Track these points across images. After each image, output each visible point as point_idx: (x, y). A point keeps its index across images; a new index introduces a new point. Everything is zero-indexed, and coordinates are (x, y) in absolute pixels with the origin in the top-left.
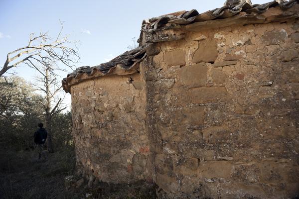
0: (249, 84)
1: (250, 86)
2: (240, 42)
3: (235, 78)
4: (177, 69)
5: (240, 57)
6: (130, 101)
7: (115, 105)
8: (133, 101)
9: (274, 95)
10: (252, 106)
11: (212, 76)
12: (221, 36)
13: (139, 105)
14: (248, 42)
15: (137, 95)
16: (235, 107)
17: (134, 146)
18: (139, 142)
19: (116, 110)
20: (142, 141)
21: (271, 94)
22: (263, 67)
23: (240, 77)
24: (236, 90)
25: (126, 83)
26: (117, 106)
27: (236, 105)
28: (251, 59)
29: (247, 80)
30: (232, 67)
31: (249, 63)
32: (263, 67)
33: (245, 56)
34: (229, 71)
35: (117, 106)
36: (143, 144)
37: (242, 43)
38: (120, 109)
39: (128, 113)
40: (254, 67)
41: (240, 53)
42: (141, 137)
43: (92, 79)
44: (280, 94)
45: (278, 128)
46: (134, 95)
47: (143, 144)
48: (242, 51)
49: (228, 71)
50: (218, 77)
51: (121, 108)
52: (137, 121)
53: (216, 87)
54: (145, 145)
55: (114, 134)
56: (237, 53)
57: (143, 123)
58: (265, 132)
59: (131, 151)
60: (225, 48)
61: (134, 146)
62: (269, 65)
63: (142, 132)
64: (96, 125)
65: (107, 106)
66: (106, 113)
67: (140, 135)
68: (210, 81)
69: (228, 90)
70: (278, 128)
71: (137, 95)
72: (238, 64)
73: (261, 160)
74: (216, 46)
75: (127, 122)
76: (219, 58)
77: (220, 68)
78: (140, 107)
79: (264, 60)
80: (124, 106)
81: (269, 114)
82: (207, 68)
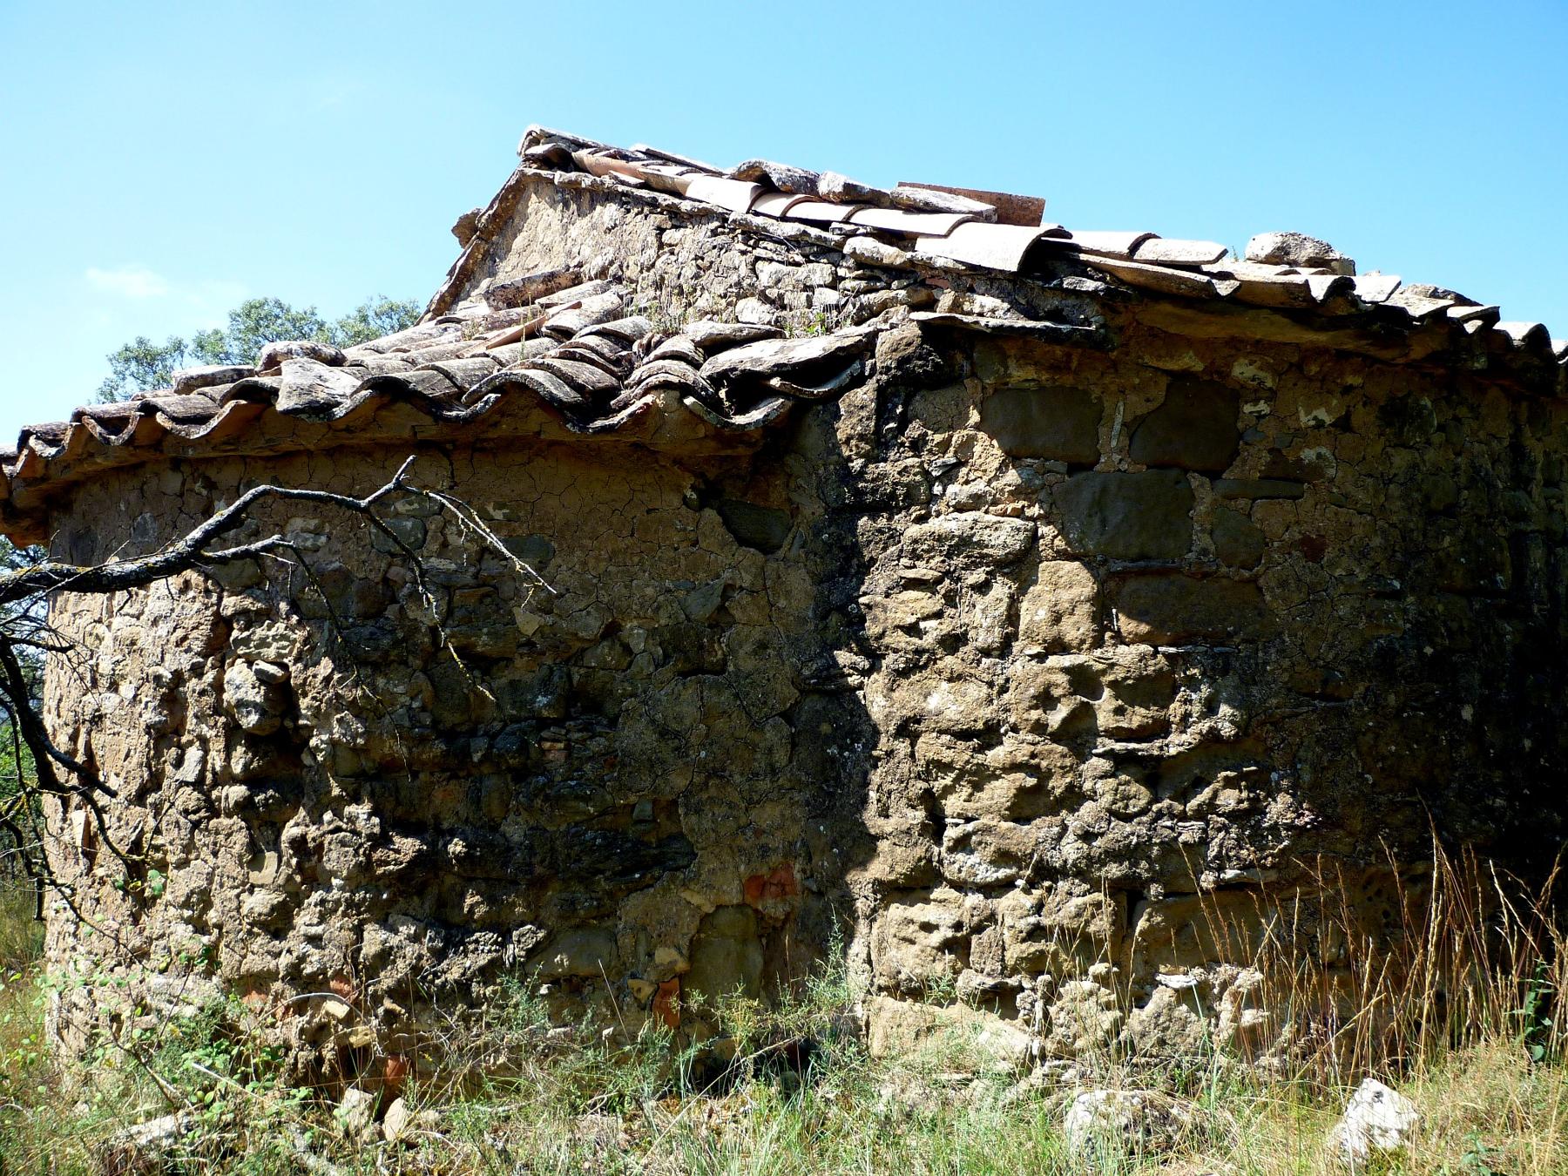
0: (1339, 580)
1: (1342, 589)
2: (1322, 414)
3: (1295, 553)
4: (1051, 478)
5: (1315, 470)
6: (701, 608)
7: (593, 624)
8: (722, 609)
9: (1405, 632)
10: (1343, 668)
11: (1211, 533)
12: (1262, 374)
13: (757, 634)
14: (1344, 424)
15: (747, 580)
16: (1293, 665)
17: (714, 864)
18: (741, 841)
19: (606, 653)
20: (759, 833)
21: (1397, 628)
22: (1380, 523)
23: (1312, 549)
24: (1296, 598)
25: (676, 501)
26: (612, 631)
27: (1298, 658)
28: (1350, 488)
29: (1333, 564)
30: (1288, 505)
31: (1343, 501)
32: (1380, 523)
33: (1331, 472)
34: (1273, 518)
35: (612, 631)
36: (765, 851)
37: (1328, 420)
38: (627, 649)
39: (684, 674)
40: (1356, 519)
41: (1319, 456)
42: (754, 814)
43: (85, 585)
44: (1423, 629)
45: (1411, 750)
46: (727, 575)
47: (765, 851)
48: (1323, 450)
49: (1273, 520)
50: (1236, 540)
51: (638, 645)
52: (738, 720)
53: (1225, 582)
54: (775, 859)
55: (587, 799)
56: (1309, 455)
57: (774, 735)
58: (1380, 765)
59: (686, 895)
60: (1270, 429)
61: (714, 864)
62: (1394, 519)
63: (764, 785)
64: (440, 747)
65: (540, 630)
66: (521, 669)
67: (751, 803)
68: (1205, 552)
69: (1268, 598)
70: (1411, 750)
71: (747, 580)
72: (1307, 502)
73: (1364, 871)
74: (1237, 412)
75: (674, 726)
76: (1244, 462)
77: (1242, 503)
78: (762, 646)
79: (1382, 498)
80: (652, 633)
81: (1392, 698)
82: (1193, 497)
